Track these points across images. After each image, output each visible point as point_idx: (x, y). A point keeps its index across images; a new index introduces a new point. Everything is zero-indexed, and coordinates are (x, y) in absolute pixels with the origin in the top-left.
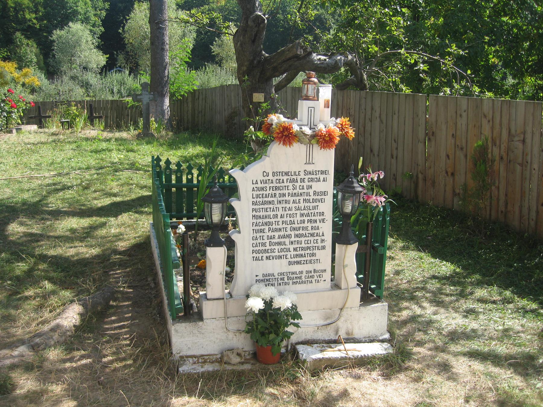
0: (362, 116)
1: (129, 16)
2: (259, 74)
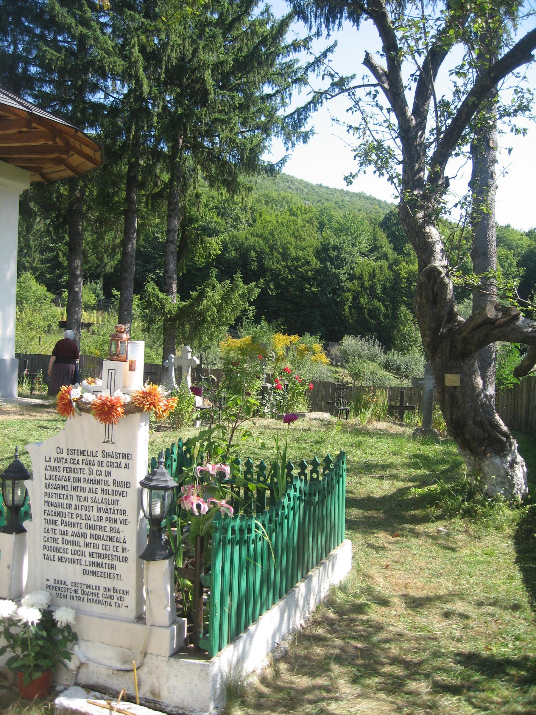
2: (449, 347)
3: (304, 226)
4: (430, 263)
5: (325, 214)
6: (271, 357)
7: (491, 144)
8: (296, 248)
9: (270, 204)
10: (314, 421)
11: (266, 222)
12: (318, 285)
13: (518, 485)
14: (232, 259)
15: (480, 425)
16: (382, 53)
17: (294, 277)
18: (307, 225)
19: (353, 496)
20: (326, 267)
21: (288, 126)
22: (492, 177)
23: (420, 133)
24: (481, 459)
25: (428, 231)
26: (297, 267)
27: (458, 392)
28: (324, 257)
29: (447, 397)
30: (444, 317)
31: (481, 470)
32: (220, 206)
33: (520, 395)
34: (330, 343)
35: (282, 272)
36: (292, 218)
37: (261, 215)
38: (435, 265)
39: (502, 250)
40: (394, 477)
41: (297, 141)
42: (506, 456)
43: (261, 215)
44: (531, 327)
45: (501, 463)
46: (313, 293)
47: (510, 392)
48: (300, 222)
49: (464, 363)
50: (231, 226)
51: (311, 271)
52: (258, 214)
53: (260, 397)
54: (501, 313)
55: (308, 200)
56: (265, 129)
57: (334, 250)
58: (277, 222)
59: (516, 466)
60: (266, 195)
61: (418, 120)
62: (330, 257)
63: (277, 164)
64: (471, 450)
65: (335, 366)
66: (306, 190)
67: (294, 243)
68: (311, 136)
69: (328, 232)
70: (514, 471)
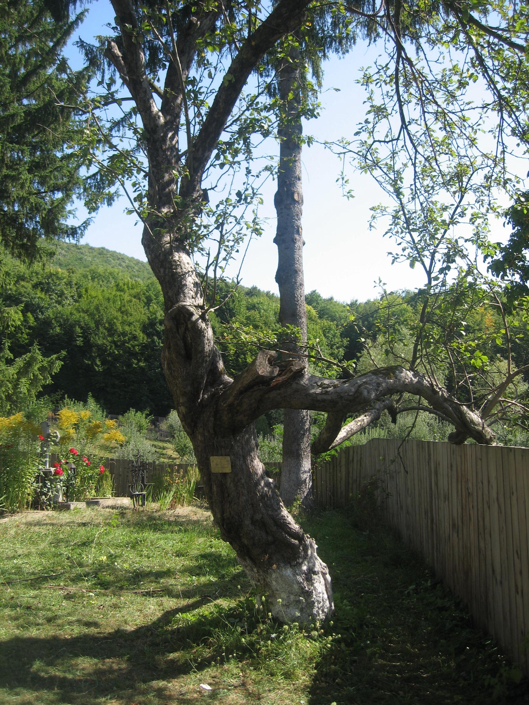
0: (480, 493)
1: (361, 353)
2: (212, 419)
3: (131, 301)
4: (178, 302)
5: (152, 289)
6: (54, 437)
7: (296, 197)
8: (123, 323)
9: (96, 280)
10: (108, 510)
11: (92, 298)
12: (146, 360)
13: (319, 602)
14: (57, 335)
15: (262, 525)
16: (114, 25)
17: (121, 352)
18: (134, 300)
19: (93, 630)
20: (153, 341)
21: (91, 187)
22: (298, 232)
23: (170, 135)
24: (266, 572)
25: (176, 258)
26: (125, 342)
27: (229, 480)
28: (151, 332)
29: (215, 488)
30: (202, 377)
31: (267, 585)
32: (44, 281)
33: (338, 468)
34: (160, 418)
35: (108, 348)
36: (118, 293)
37: (86, 291)
38: (184, 303)
39: (325, 321)
40: (168, 592)
41: (101, 203)
42: (300, 564)
43: (86, 291)
44: (320, 386)
45: (294, 575)
46: (141, 368)
47: (328, 465)
48: (126, 297)
49: (235, 440)
50: (56, 302)
51: (138, 346)
52: (84, 290)
53: (40, 484)
54: (278, 369)
55: (138, 277)
56: (67, 190)
57: (161, 324)
58: (103, 297)
59: (315, 577)
60: (93, 270)
61: (168, 118)
62: (157, 331)
63: (79, 227)
64: (251, 559)
65: (163, 441)
66: (136, 268)
67: (120, 318)
68: (115, 198)
69: (155, 307)
70: (312, 584)
